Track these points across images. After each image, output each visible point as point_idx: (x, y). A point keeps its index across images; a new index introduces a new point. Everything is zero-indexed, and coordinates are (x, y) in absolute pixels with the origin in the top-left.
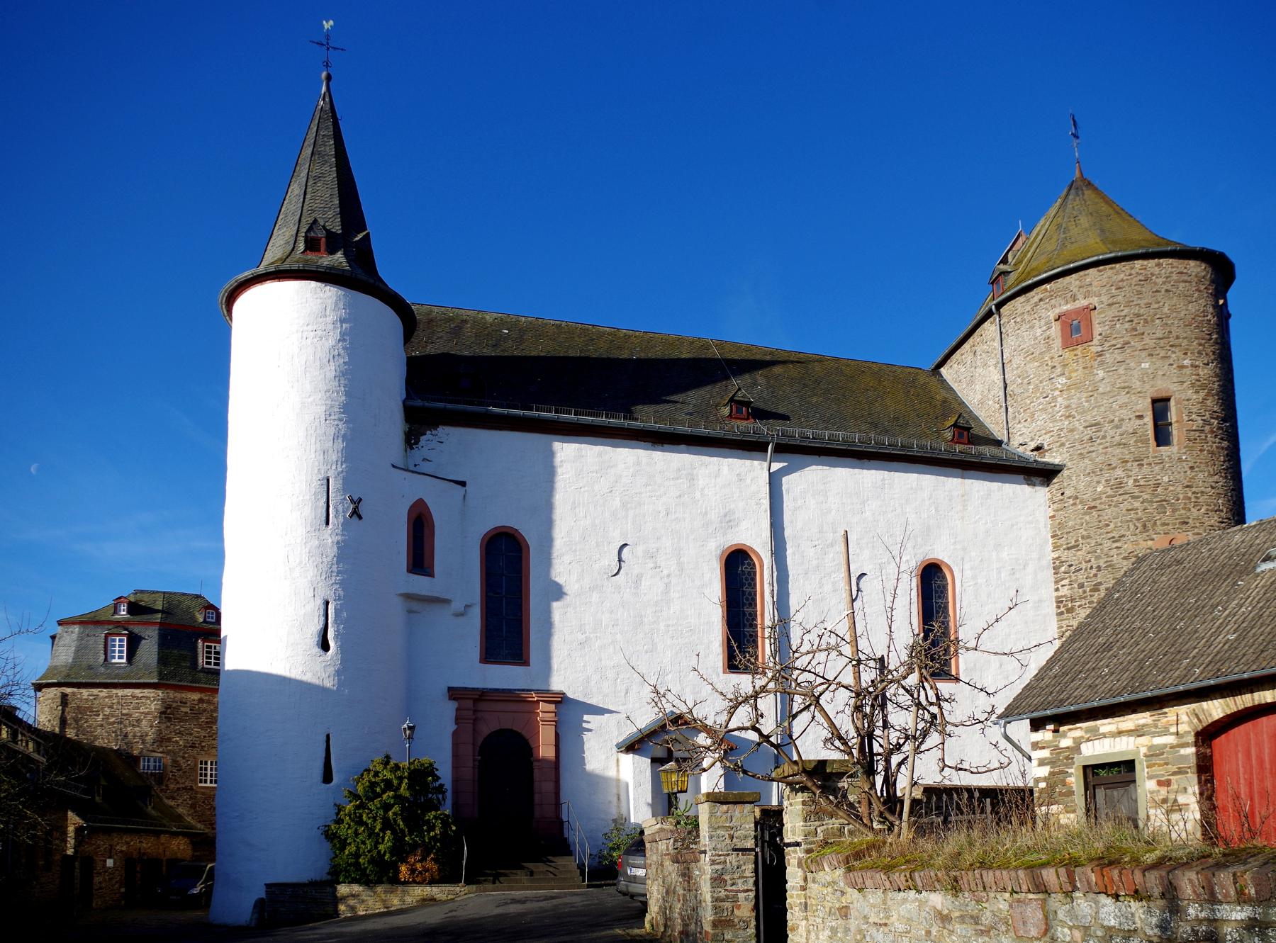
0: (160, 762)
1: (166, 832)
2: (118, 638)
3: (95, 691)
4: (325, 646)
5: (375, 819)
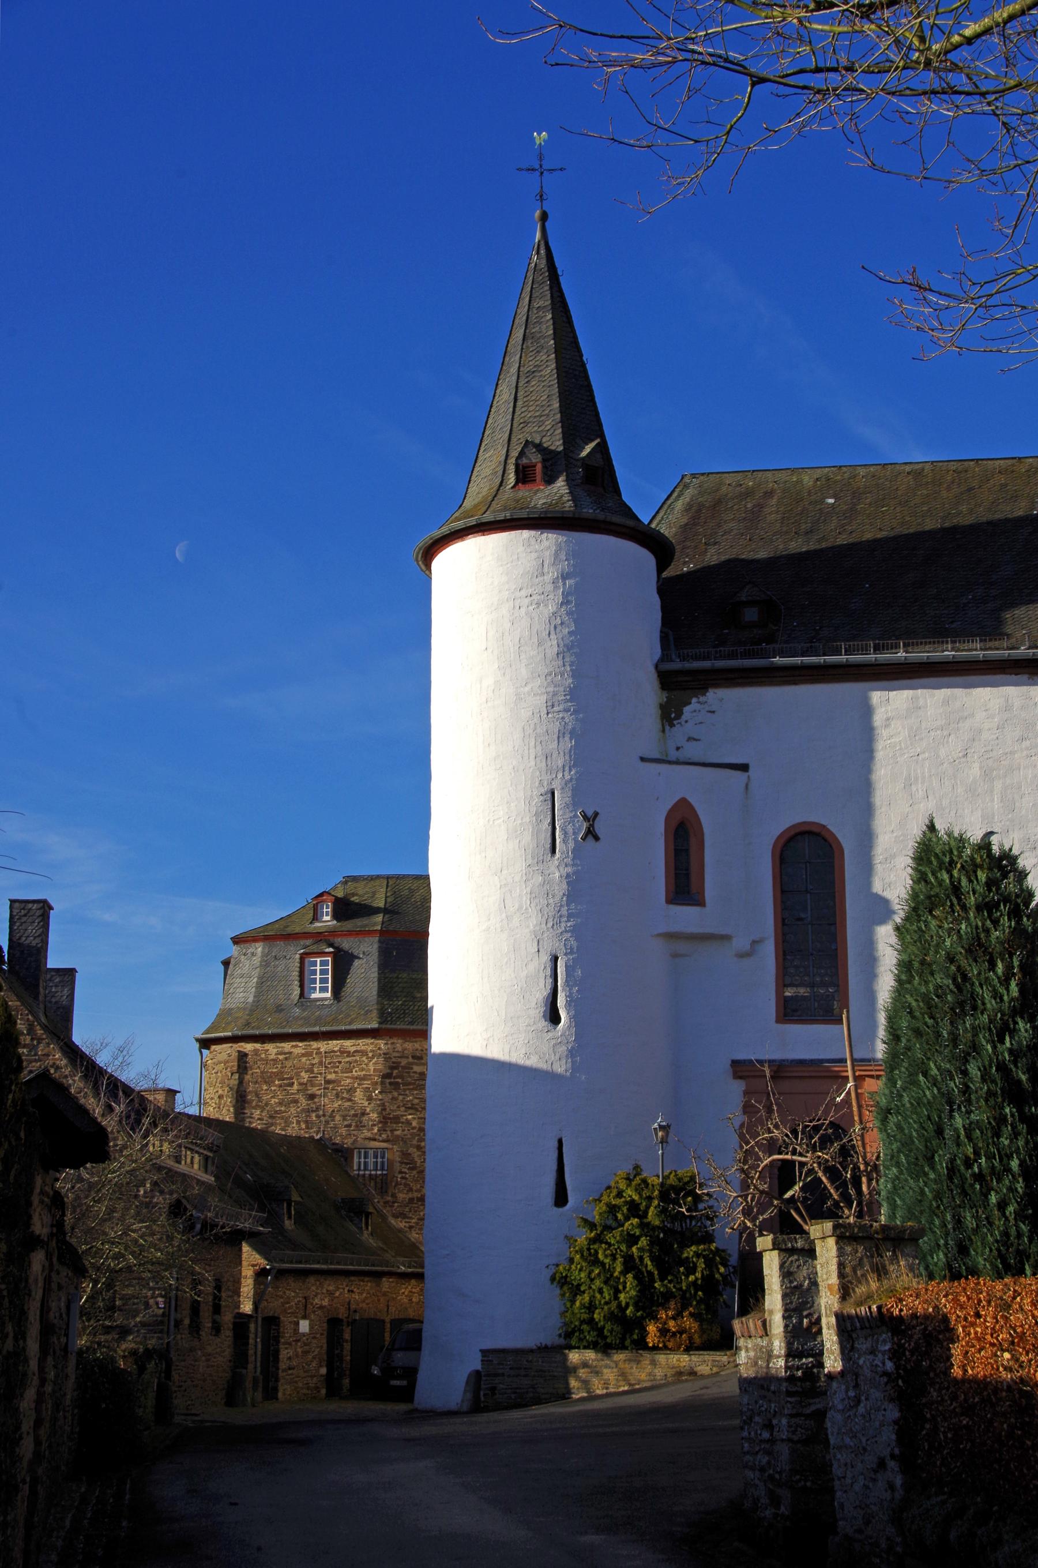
0: (383, 1157)
1: (390, 1274)
2: (318, 960)
3: (287, 1046)
4: (554, 1017)
5: (614, 1258)
